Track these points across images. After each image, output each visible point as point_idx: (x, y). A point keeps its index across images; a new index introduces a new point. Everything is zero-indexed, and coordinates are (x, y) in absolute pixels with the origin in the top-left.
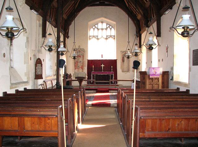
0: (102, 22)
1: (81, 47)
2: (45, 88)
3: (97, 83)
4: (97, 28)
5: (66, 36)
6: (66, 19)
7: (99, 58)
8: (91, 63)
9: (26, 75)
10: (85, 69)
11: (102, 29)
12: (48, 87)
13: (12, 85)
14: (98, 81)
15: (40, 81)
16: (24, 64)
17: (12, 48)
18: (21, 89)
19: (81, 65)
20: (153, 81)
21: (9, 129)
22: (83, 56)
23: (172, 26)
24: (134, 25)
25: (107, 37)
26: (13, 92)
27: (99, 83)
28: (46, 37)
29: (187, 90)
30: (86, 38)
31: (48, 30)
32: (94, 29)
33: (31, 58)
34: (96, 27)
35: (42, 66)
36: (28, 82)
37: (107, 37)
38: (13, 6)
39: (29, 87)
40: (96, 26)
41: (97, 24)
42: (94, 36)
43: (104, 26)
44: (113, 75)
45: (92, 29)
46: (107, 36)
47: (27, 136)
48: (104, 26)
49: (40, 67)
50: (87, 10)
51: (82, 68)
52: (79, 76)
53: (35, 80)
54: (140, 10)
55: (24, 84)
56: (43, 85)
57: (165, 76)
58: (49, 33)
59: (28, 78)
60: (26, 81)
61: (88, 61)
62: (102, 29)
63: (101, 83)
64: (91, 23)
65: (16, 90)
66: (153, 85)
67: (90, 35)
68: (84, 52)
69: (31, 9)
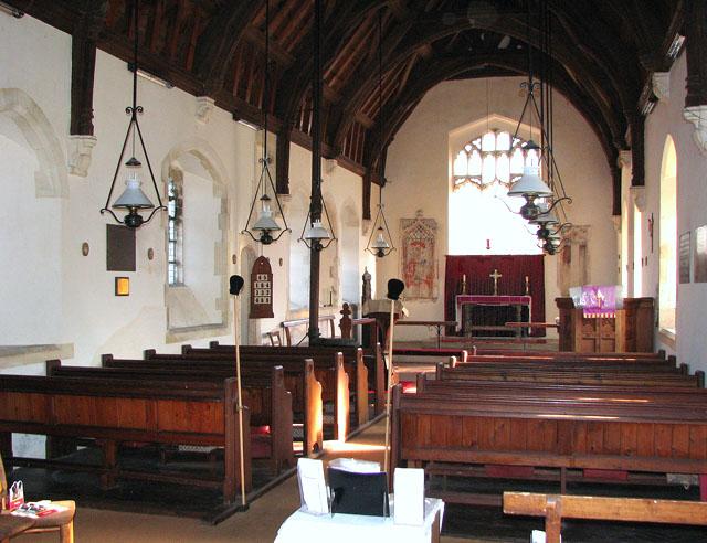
0: (496, 131)
1: (426, 216)
2: (286, 345)
3: (476, 333)
4: (480, 151)
6: (368, 126)
7: (479, 250)
8: (457, 265)
9: (218, 306)
10: (437, 286)
11: (496, 154)
12: (295, 342)
13: (173, 333)
14: (476, 328)
15: (266, 325)
16: (215, 274)
17: (181, 229)
18: (201, 343)
19: (427, 271)
20: (595, 330)
21: (129, 426)
22: (432, 243)
24: (599, 144)
25: (513, 181)
26: (175, 349)
27: (485, 333)
30: (439, 183)
32: (468, 153)
33: (234, 257)
34: (474, 146)
35: (270, 278)
36: (226, 327)
37: (513, 181)
38: (140, 158)
39: (228, 339)
40: (476, 143)
41: (481, 137)
42: (468, 178)
43: (504, 141)
44: (530, 306)
45: (462, 153)
46: (512, 176)
48: (504, 141)
49: (265, 284)
50: (444, 93)
51: (429, 282)
52: (380, 311)
53: (251, 320)
54: (599, 92)
55: (209, 332)
56: (277, 334)
57: (640, 315)
59: (225, 315)
60: (220, 322)
61: (450, 259)
62: (496, 154)
63: (490, 333)
64: (455, 134)
65: (183, 347)
66: (597, 343)
67: (456, 174)
68: (434, 229)
69: (236, 118)
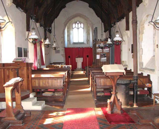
5: (50, 31)
23: (151, 21)
28: (30, 31)
29: (142, 73)
31: (31, 25)
47: (73, 95)
55: (149, 71)
58: (32, 28)
